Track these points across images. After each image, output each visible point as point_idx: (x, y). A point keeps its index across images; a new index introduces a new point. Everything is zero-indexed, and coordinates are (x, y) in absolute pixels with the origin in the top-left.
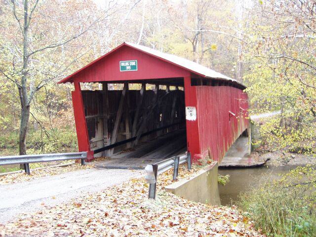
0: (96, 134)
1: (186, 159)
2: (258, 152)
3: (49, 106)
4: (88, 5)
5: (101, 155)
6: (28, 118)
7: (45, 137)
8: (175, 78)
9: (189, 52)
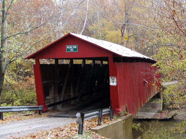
0: (50, 94)
1: (109, 111)
2: (168, 109)
3: (18, 73)
4: (49, 3)
5: (53, 108)
6: (3, 82)
7: (14, 95)
8: (101, 57)
9: (119, 37)
